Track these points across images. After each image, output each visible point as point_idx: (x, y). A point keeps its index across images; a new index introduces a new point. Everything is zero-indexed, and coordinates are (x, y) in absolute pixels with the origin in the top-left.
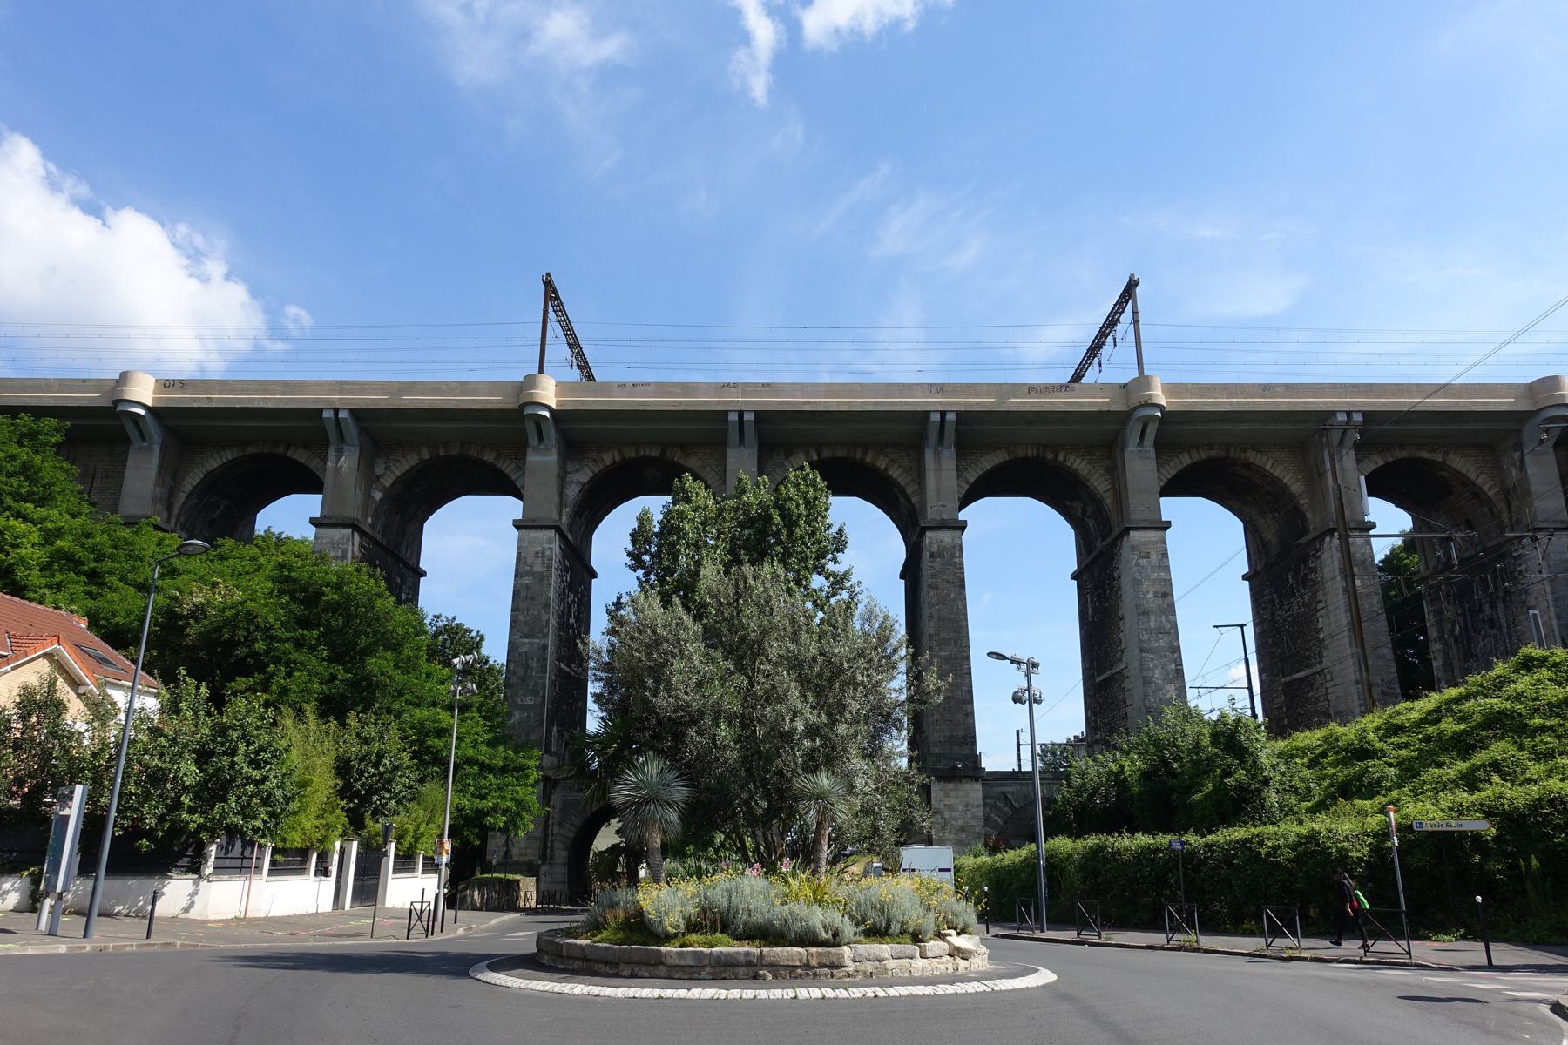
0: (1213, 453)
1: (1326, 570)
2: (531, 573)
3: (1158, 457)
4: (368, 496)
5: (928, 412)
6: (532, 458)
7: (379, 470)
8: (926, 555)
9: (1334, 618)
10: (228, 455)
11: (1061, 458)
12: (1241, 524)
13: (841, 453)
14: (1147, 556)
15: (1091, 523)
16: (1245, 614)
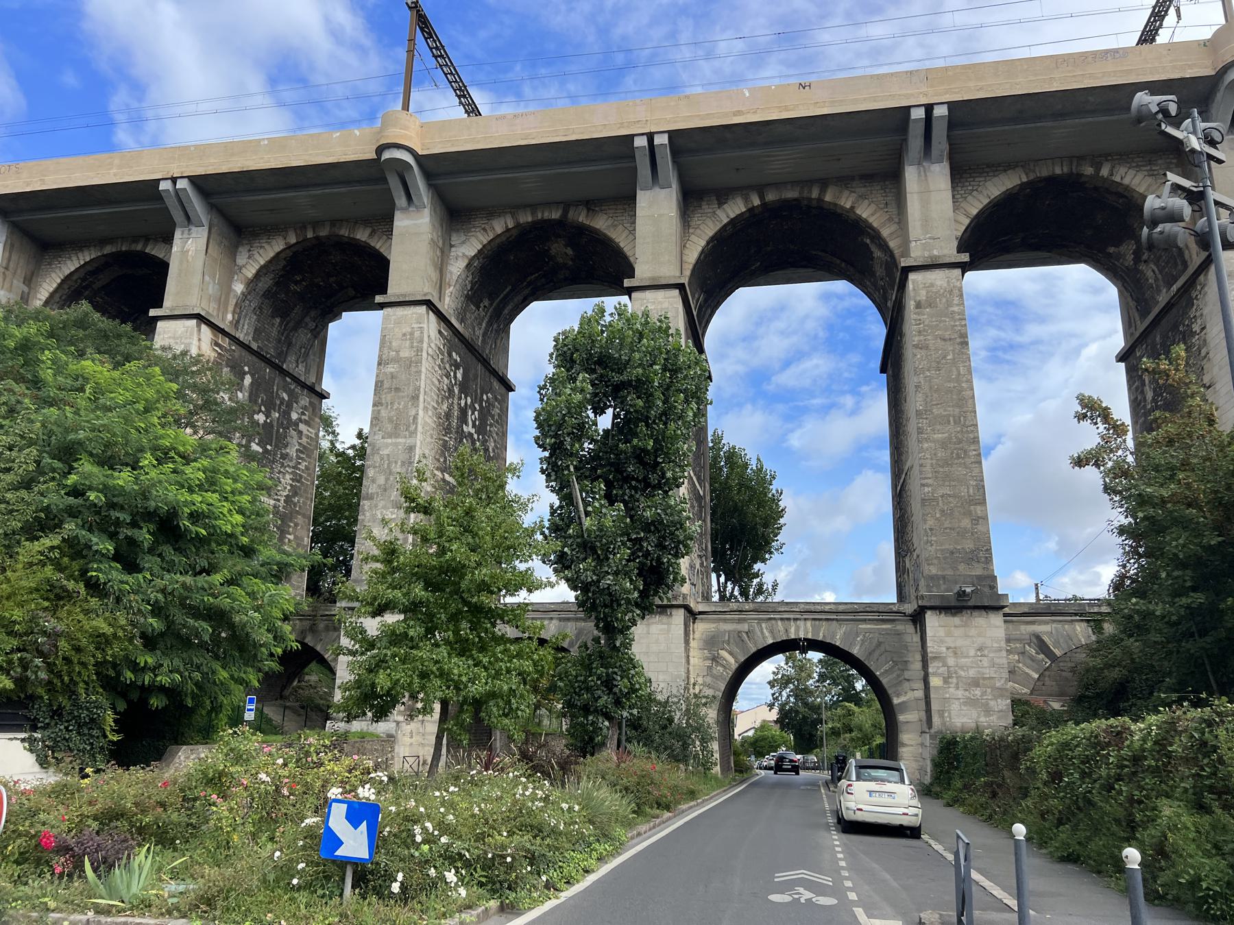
2: (397, 360)
4: (226, 288)
5: (907, 109)
6: (401, 222)
7: (241, 260)
10: (86, 257)
11: (1105, 172)
13: (791, 194)
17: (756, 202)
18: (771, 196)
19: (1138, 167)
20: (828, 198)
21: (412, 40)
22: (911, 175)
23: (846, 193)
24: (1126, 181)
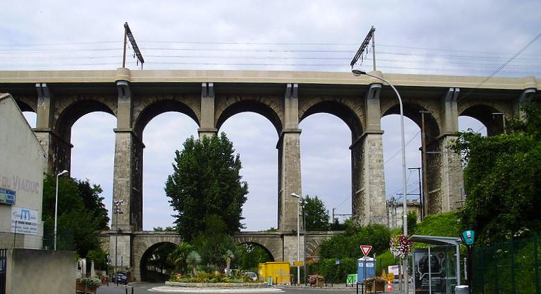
6: (120, 102)
7: (57, 106)
8: (285, 143)
11: (343, 101)
13: (250, 98)
15: (356, 128)
17: (239, 100)
18: (244, 98)
20: (262, 101)
21: (125, 39)
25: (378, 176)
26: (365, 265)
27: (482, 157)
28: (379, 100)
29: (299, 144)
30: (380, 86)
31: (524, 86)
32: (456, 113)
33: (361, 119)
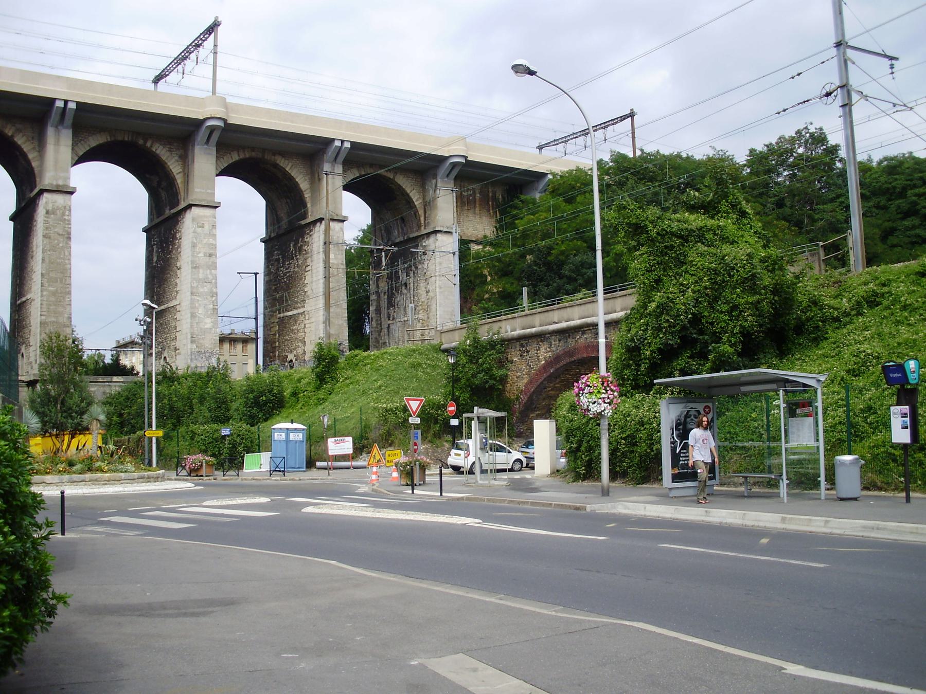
0: (254, 154)
1: (315, 245)
3: (217, 152)
9: (314, 279)
11: (148, 144)
12: (264, 202)
14: (202, 227)
15: (163, 194)
16: (259, 264)
19: (164, 145)
22: (50, 132)
23: (9, 126)
24: (158, 152)
25: (206, 281)
26: (287, 436)
27: (666, 247)
28: (215, 149)
29: (70, 215)
30: (221, 124)
31: (449, 151)
32: (339, 181)
33: (179, 180)
